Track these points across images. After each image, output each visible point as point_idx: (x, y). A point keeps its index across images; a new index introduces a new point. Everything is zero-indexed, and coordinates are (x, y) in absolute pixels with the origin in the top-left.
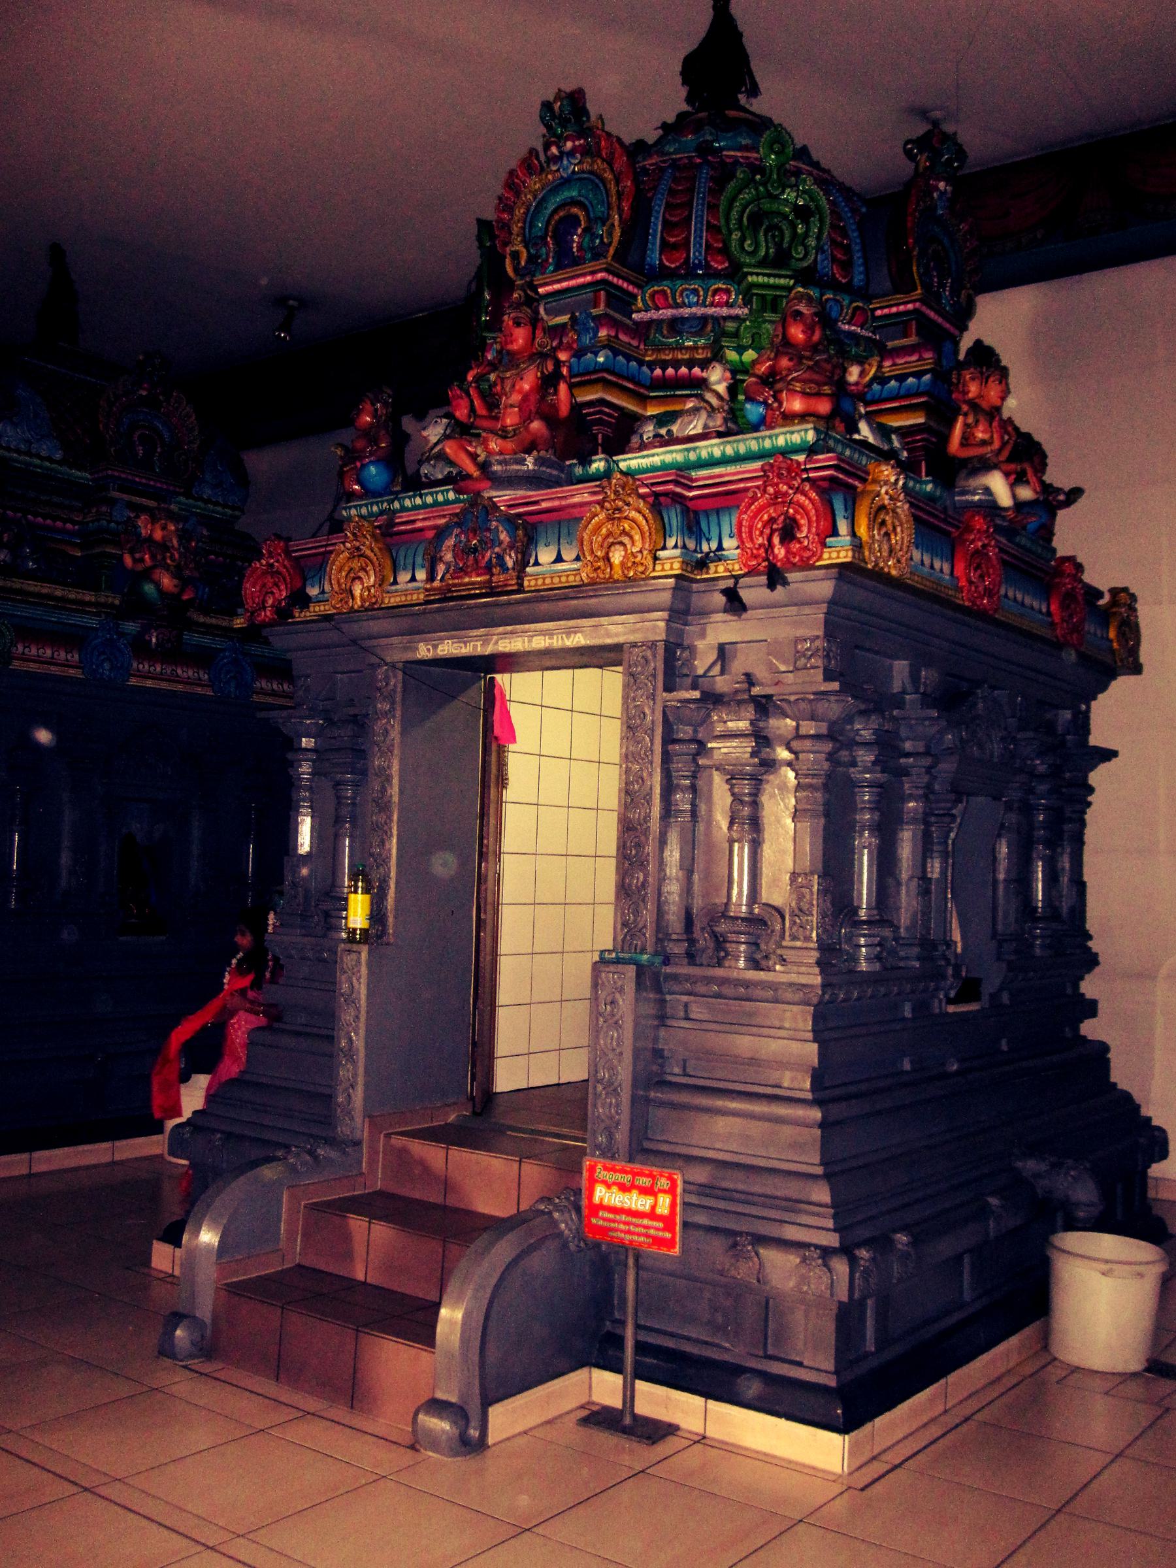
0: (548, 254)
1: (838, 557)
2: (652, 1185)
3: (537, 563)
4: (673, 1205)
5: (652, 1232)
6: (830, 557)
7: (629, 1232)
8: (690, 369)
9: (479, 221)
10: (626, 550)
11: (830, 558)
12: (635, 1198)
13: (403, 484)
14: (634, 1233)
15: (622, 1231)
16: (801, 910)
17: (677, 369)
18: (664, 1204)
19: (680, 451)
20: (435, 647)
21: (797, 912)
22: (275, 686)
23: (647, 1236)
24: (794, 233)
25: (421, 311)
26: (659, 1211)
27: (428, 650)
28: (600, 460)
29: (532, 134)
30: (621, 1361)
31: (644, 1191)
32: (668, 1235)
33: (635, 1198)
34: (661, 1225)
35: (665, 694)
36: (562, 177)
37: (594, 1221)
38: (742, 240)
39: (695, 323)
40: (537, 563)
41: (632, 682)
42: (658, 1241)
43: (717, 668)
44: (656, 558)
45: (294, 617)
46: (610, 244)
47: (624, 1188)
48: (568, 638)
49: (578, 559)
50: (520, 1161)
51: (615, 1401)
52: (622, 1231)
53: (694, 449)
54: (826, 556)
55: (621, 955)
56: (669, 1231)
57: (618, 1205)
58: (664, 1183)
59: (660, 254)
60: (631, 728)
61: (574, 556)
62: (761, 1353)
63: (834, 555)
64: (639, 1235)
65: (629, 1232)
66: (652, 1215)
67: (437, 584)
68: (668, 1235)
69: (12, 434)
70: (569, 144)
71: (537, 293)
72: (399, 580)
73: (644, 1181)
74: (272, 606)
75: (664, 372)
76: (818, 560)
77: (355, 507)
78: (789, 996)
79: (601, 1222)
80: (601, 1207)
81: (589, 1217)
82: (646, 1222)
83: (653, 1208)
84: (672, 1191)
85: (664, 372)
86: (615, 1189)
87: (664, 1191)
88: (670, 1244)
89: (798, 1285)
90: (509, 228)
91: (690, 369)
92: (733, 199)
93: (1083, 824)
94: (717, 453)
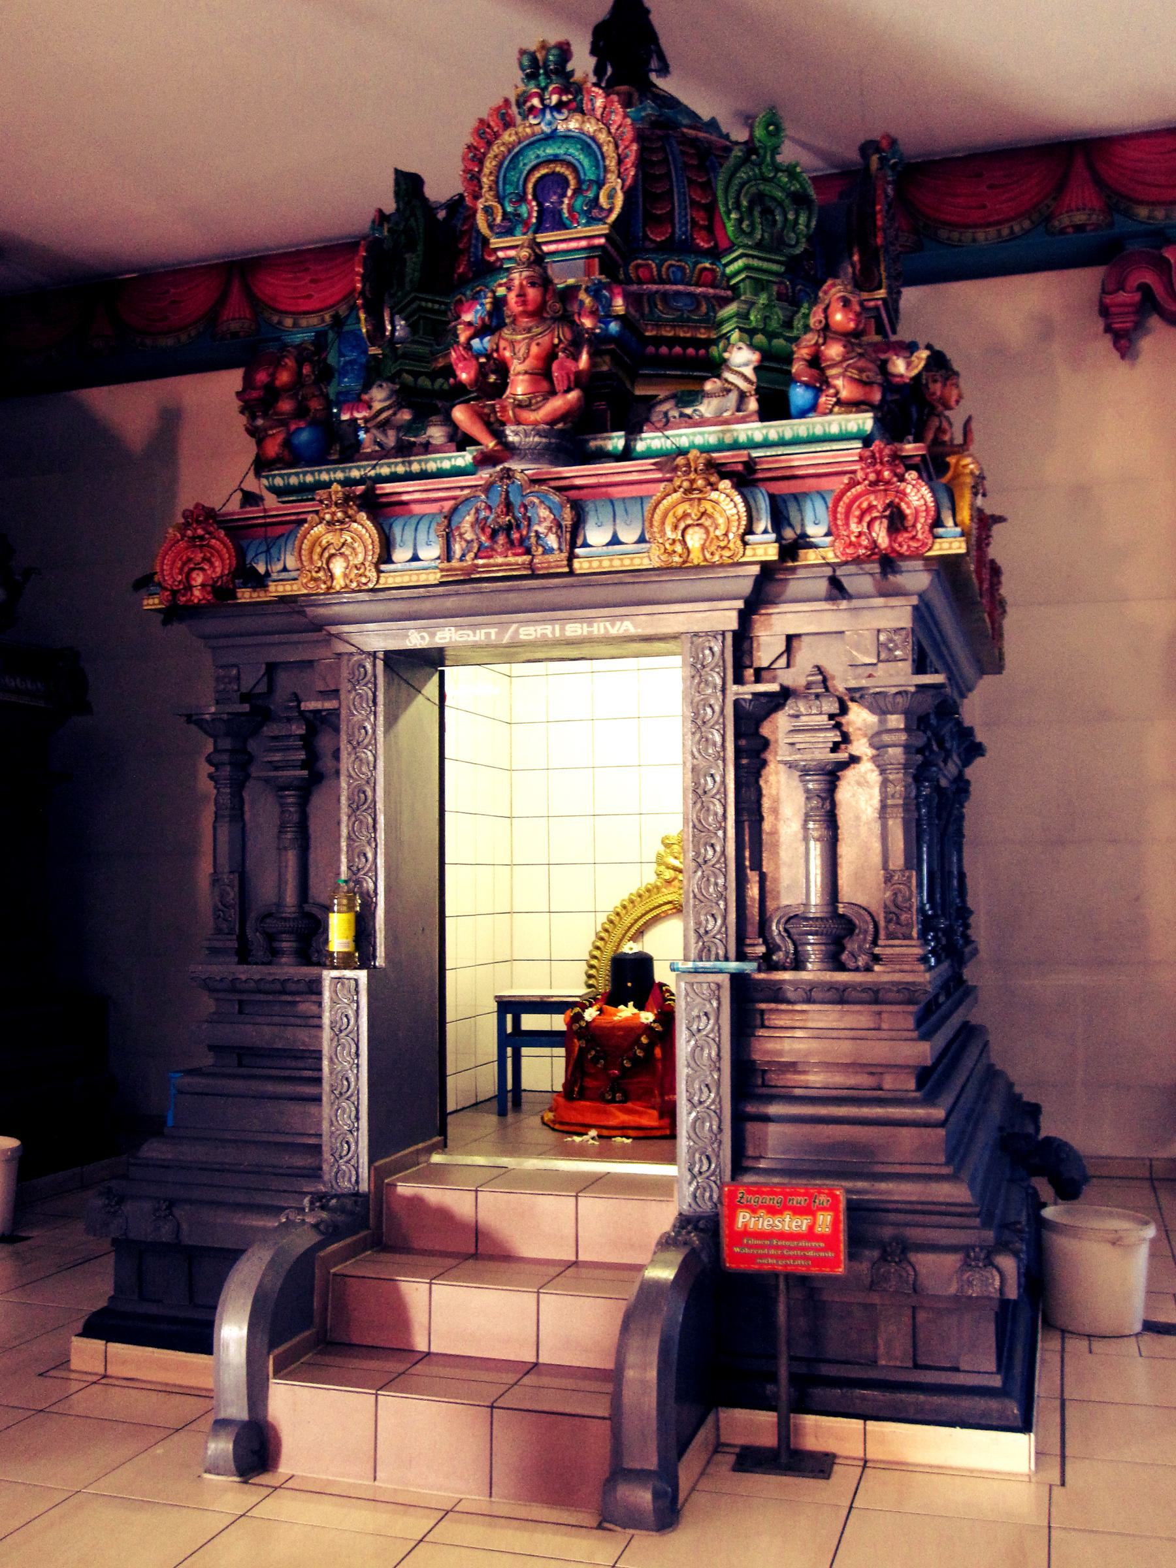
0: (530, 214)
1: (950, 548)
2: (809, 1204)
3: (585, 545)
4: (835, 1222)
5: (811, 1253)
6: (941, 548)
7: (783, 1257)
8: (684, 349)
9: (398, 172)
10: (707, 532)
11: (940, 549)
12: (787, 1219)
13: (341, 453)
14: (789, 1257)
15: (772, 1256)
16: (897, 906)
17: (671, 348)
18: (824, 1222)
19: (714, 432)
20: (432, 635)
21: (894, 909)
22: (29, 686)
23: (806, 1258)
24: (786, 219)
25: (134, 272)
26: (818, 1230)
27: (423, 638)
28: (619, 438)
29: (509, 81)
30: (776, 1396)
31: (798, 1211)
32: (830, 1254)
33: (787, 1219)
34: (822, 1245)
35: (735, 687)
36: (543, 132)
37: (737, 1250)
38: (740, 221)
39: (688, 301)
40: (585, 545)
41: (697, 669)
42: (818, 1262)
43: (783, 662)
44: (745, 544)
45: (236, 598)
46: (611, 210)
47: (773, 1211)
48: (613, 626)
49: (642, 540)
50: (577, 1197)
51: (769, 1439)
52: (772, 1256)
53: (729, 431)
54: (936, 546)
55: (700, 964)
56: (831, 1250)
57: (767, 1228)
58: (823, 1199)
59: (644, 227)
60: (698, 724)
61: (635, 537)
62: (910, 1364)
63: (946, 546)
64: (795, 1258)
65: (783, 1257)
66: (811, 1235)
67: (455, 563)
68: (830, 1254)
69: (1174, 309)
70: (555, 99)
71: (541, 250)
72: (395, 557)
73: (799, 1201)
74: (203, 585)
75: (657, 350)
76: (929, 550)
77: (281, 475)
78: (892, 996)
79: (747, 1251)
80: (746, 1233)
81: (730, 1247)
82: (803, 1244)
83: (811, 1228)
84: (833, 1208)
85: (657, 350)
86: (762, 1213)
87: (824, 1209)
88: (835, 1263)
89: (961, 1289)
90: (479, 181)
91: (684, 349)
92: (732, 175)
93: (961, 818)
94: (758, 437)
